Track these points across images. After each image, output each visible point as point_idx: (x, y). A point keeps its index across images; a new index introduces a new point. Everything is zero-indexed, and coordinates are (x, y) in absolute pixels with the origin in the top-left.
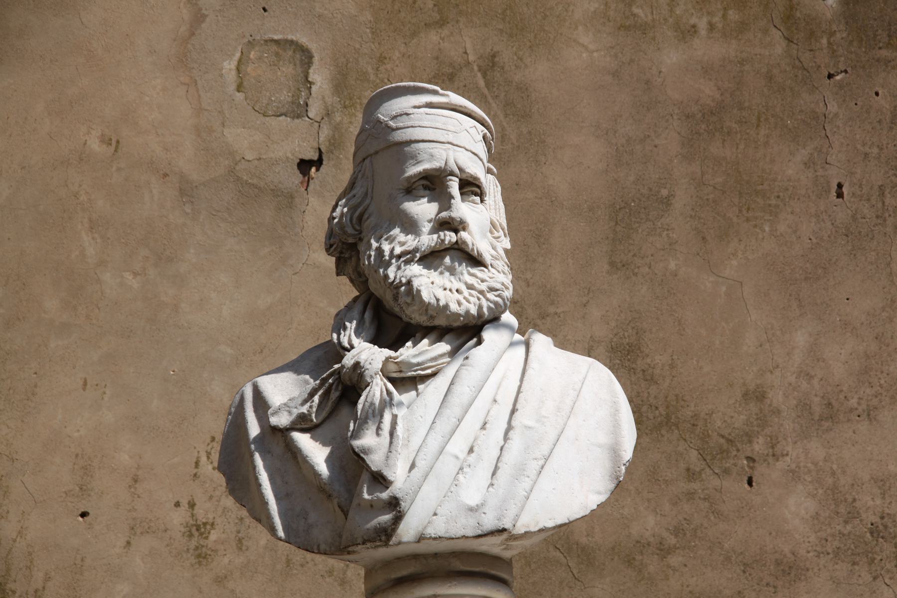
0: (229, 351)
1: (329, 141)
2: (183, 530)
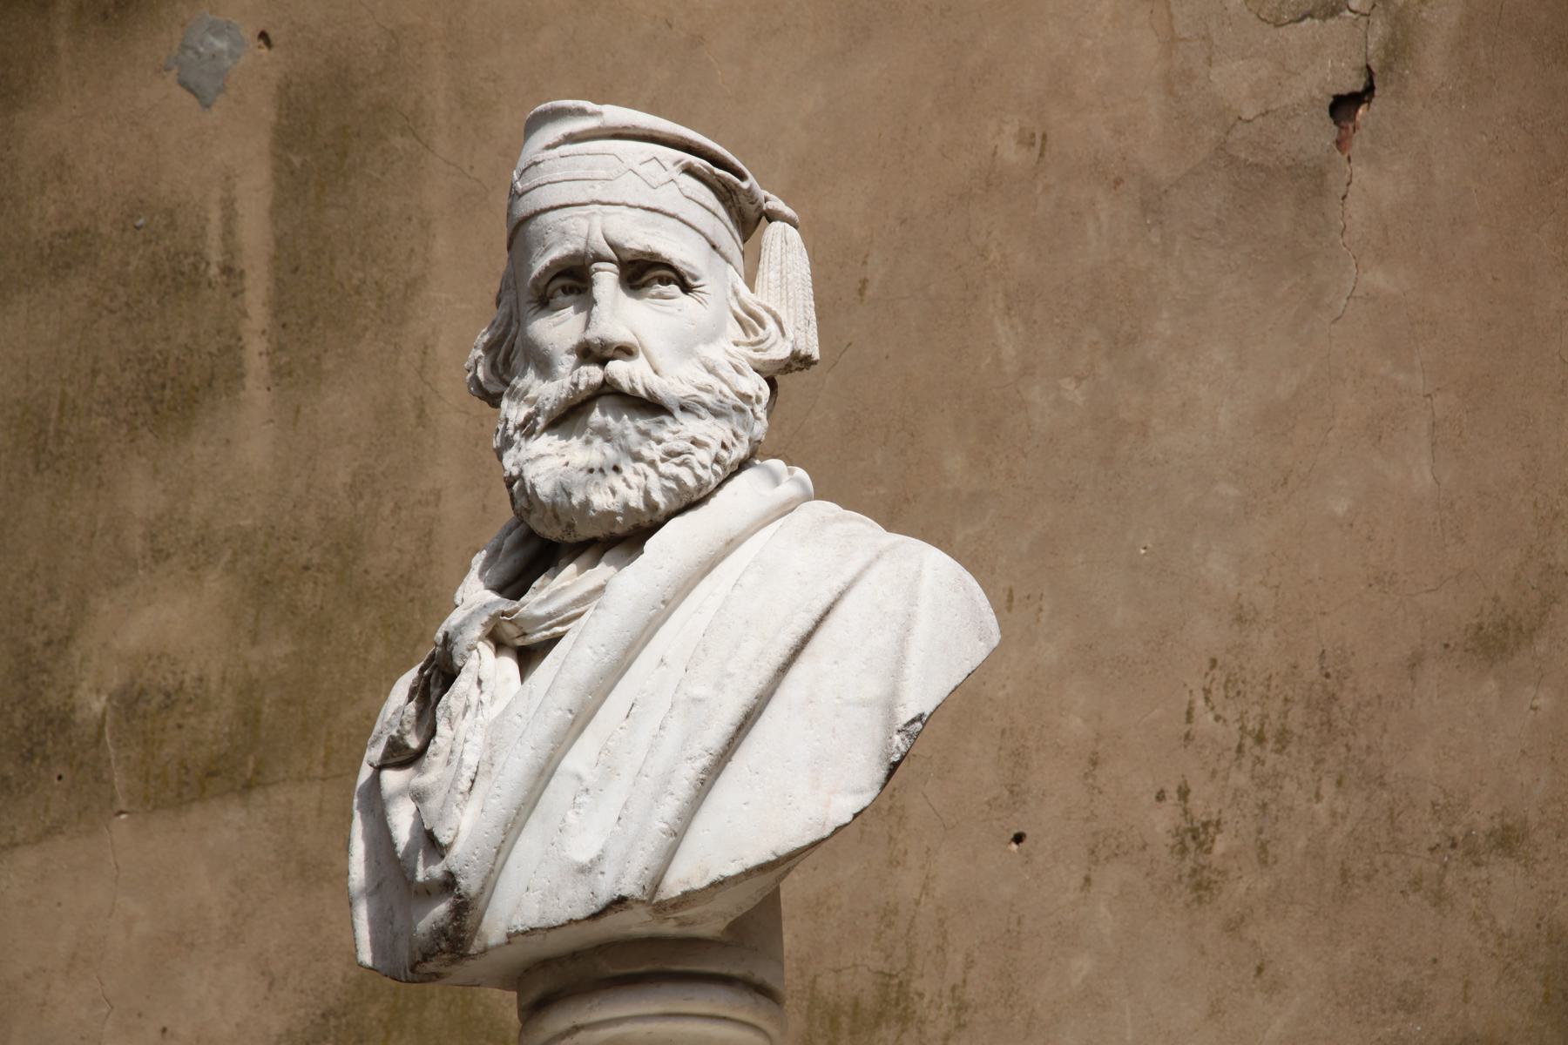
0: (1232, 492)
1: (1386, 48)
2: (1171, 841)
